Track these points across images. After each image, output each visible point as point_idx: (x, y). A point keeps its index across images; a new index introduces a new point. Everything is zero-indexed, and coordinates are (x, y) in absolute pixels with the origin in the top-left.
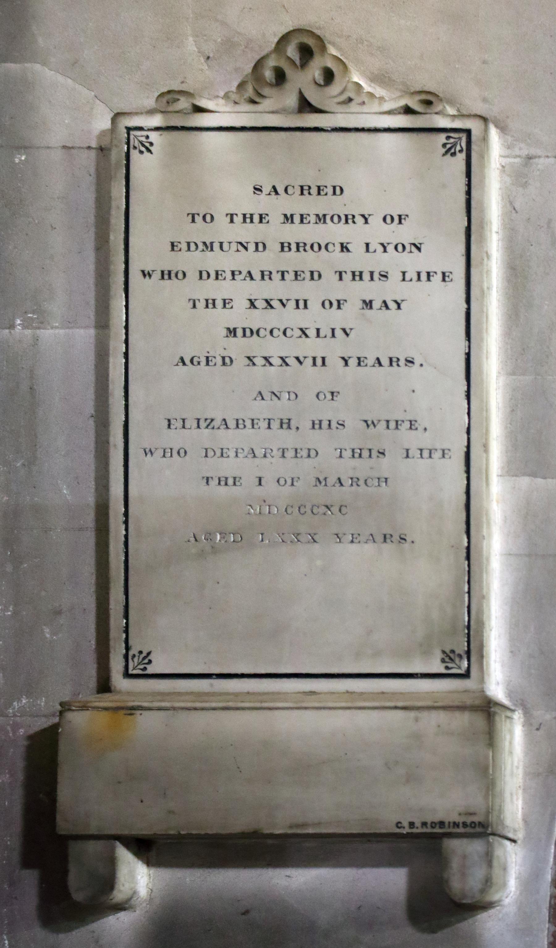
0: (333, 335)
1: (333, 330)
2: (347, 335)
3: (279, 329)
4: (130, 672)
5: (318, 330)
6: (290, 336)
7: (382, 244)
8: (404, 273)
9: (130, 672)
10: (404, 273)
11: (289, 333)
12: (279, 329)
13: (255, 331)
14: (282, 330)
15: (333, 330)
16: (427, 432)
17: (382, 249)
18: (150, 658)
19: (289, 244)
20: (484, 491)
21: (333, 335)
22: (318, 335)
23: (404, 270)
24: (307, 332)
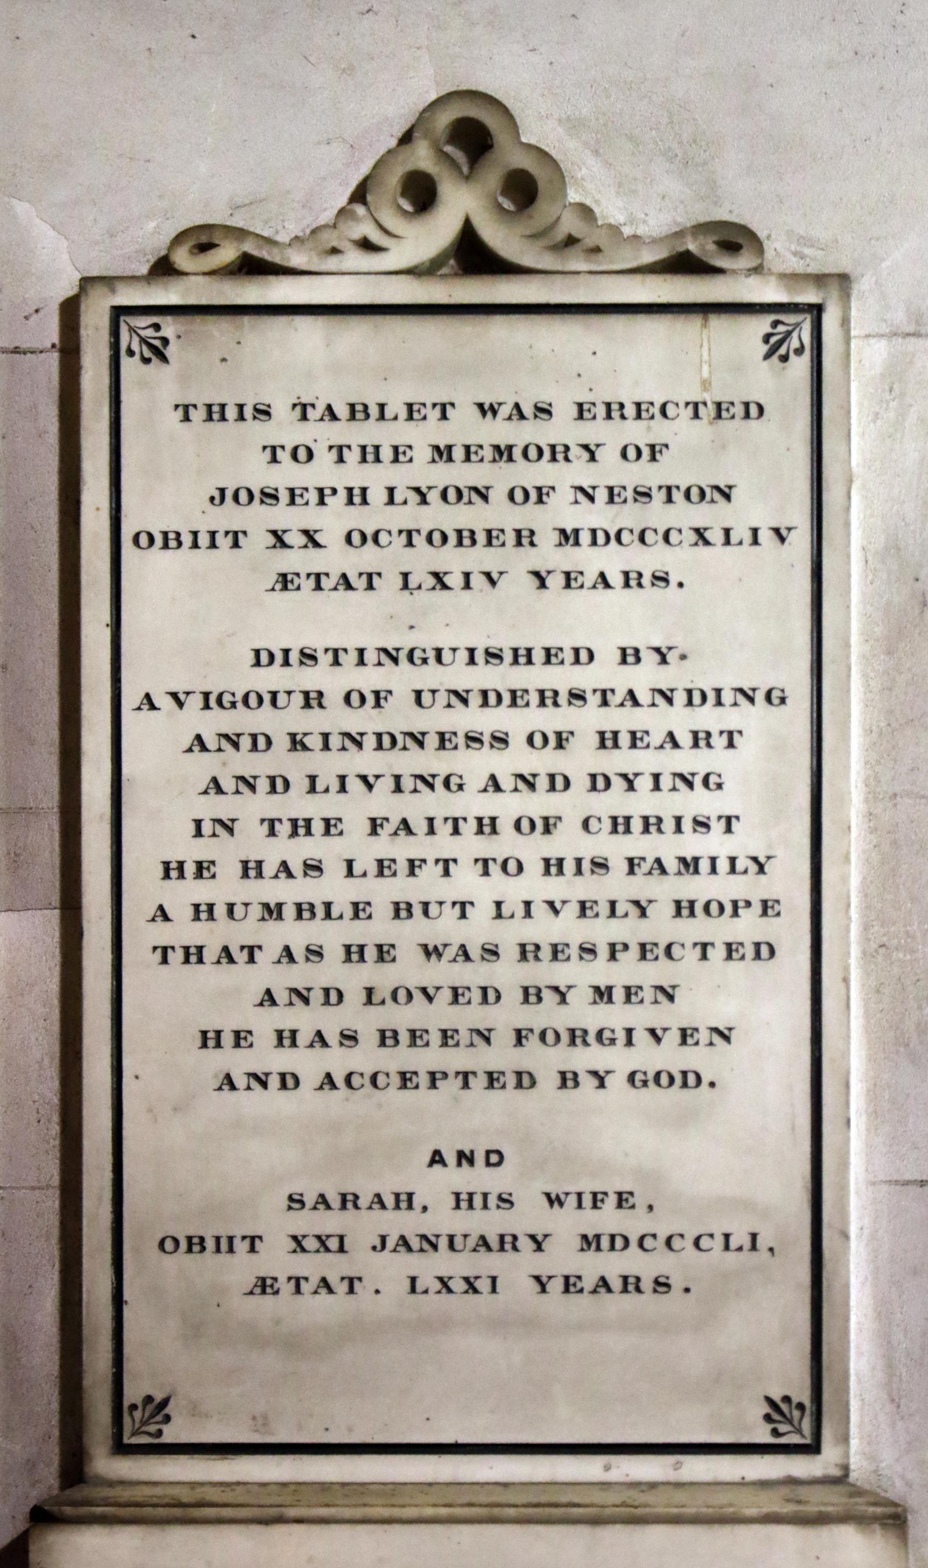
0: (755, 542)
1: (755, 531)
2: (783, 540)
3: (655, 531)
4: (126, 1440)
5: (727, 532)
6: (677, 543)
7: (417, 490)
8: (405, 576)
9: (126, 1440)
10: (405, 576)
11: (674, 537)
12: (655, 531)
13: (613, 541)
14: (661, 532)
15: (755, 531)
16: (216, 1303)
17: (417, 498)
18: (167, 1410)
19: (178, 534)
20: (816, 1509)
21: (755, 542)
22: (727, 542)
23: (405, 570)
24: (707, 535)
